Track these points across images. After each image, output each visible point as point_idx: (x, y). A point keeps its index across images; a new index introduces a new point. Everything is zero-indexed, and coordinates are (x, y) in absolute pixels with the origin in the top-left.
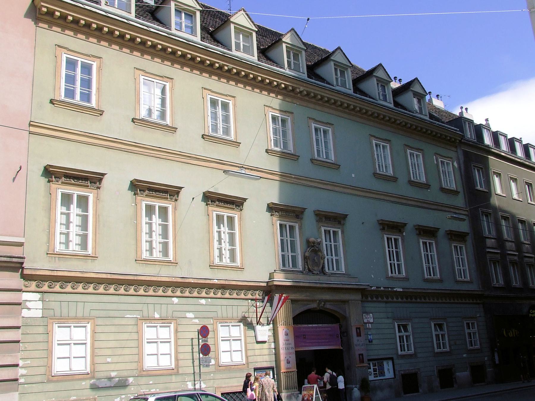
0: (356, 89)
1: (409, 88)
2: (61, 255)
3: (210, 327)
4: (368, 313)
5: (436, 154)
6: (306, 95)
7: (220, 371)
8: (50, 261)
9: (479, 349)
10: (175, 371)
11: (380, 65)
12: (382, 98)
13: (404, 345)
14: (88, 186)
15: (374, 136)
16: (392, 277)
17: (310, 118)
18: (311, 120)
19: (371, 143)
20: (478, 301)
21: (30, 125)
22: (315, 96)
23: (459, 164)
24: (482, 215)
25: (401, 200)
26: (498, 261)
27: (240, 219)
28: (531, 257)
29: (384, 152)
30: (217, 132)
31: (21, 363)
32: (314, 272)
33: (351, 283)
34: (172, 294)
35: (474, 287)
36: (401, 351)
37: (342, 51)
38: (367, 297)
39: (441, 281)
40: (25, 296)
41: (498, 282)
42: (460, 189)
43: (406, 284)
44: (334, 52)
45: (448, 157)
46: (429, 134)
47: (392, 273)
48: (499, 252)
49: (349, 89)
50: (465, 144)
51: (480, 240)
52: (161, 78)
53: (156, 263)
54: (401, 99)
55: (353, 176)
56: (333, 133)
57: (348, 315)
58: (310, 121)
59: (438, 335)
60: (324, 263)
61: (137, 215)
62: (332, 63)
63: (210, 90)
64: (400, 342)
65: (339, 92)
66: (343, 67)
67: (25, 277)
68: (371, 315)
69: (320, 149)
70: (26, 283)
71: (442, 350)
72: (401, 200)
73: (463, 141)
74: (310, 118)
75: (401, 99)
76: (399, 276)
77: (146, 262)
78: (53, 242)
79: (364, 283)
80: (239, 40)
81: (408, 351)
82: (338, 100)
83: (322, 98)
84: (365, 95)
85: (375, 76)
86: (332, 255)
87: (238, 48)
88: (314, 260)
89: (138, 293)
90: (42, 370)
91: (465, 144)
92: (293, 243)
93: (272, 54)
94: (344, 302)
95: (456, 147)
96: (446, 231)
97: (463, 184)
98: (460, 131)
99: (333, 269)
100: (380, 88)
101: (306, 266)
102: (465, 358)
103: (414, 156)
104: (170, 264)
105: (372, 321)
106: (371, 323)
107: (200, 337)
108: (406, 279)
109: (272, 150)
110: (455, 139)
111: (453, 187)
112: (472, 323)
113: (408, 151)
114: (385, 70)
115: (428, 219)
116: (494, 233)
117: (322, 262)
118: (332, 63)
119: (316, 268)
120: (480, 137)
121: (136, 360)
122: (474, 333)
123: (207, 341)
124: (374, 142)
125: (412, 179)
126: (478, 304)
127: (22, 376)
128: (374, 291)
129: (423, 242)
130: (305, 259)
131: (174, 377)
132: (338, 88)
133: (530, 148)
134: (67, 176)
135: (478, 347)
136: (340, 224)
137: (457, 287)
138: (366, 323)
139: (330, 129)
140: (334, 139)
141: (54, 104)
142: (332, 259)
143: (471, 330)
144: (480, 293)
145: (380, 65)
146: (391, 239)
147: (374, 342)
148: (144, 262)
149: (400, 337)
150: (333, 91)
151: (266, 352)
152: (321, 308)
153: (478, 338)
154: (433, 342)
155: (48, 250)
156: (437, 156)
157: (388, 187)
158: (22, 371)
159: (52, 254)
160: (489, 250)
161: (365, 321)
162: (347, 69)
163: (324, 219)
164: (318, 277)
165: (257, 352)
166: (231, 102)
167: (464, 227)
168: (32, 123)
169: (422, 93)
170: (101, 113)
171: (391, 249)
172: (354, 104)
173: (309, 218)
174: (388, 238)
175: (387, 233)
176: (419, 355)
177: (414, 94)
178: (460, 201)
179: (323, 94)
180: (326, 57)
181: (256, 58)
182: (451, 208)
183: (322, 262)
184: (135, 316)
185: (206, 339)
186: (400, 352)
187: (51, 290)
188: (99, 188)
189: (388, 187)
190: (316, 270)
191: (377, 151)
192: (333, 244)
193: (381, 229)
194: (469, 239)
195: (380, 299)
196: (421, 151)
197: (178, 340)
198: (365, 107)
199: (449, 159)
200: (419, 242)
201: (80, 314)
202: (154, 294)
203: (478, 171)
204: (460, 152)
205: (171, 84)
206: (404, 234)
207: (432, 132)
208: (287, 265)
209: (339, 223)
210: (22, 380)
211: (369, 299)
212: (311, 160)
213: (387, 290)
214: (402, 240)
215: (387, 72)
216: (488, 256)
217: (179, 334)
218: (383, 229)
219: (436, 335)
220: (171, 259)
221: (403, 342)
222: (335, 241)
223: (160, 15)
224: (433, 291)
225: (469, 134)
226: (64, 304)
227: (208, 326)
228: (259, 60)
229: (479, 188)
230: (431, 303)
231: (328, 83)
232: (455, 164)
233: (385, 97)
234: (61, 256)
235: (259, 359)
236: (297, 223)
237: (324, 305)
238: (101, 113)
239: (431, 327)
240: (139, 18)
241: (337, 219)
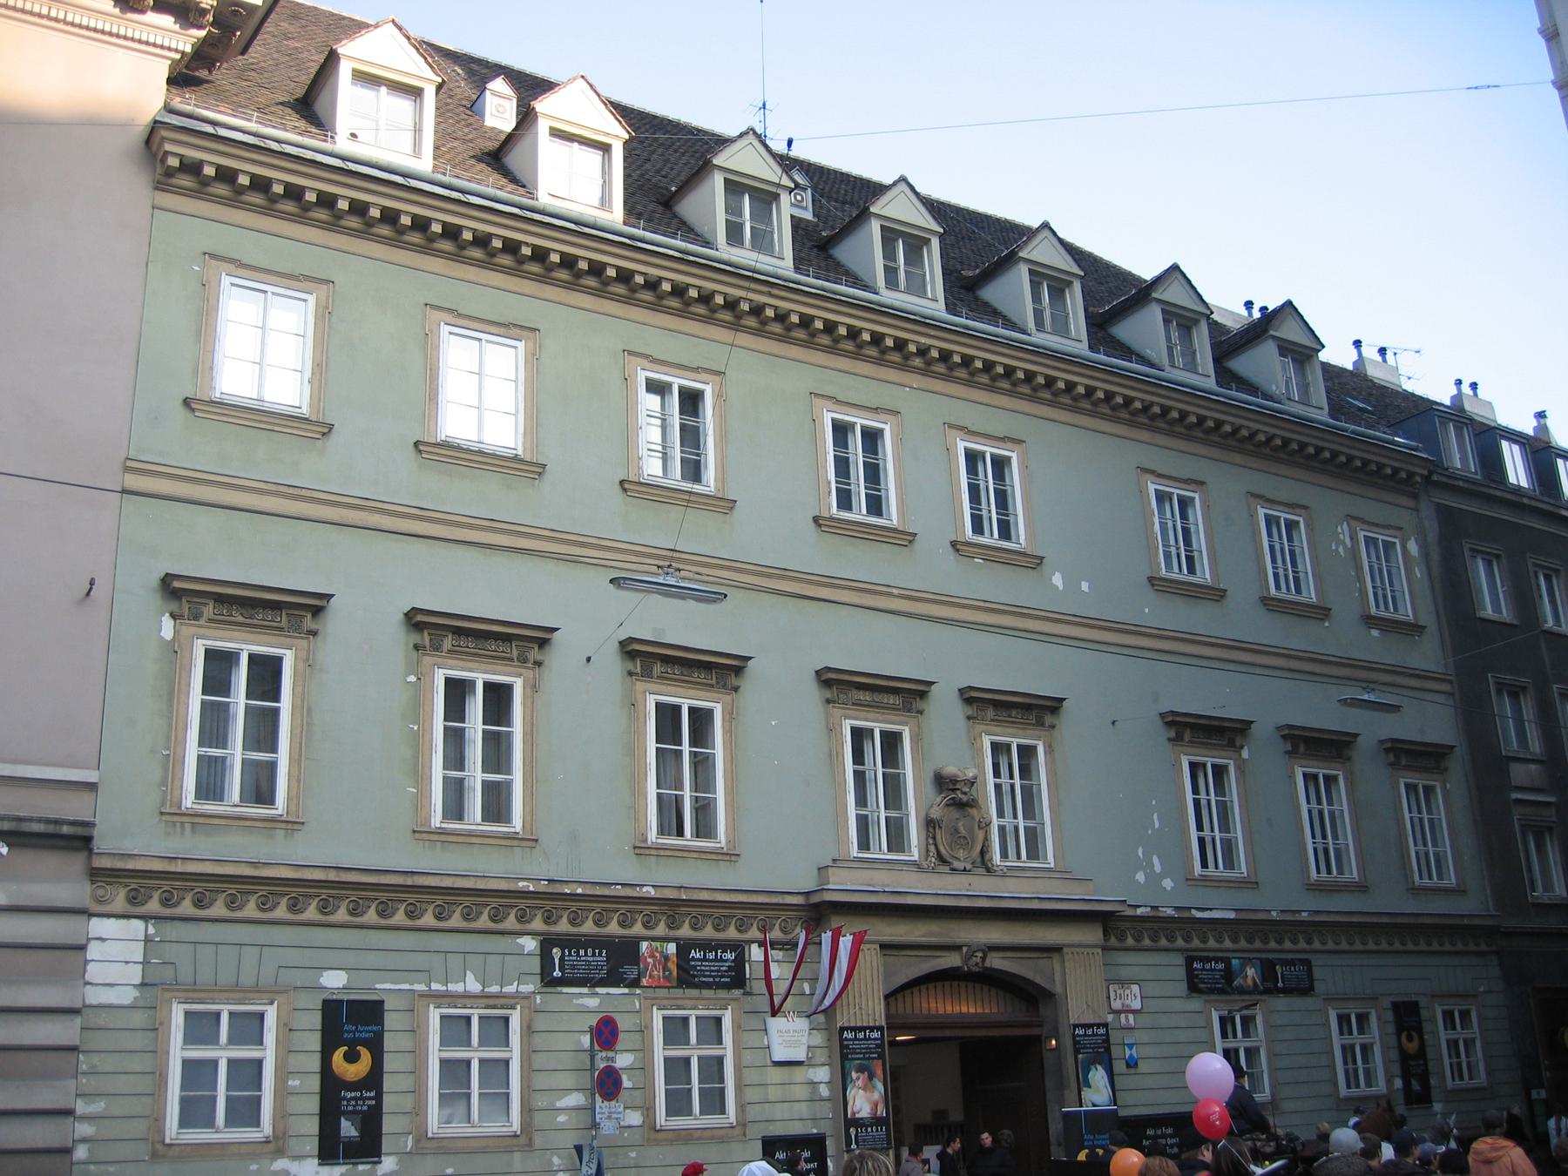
0: (1226, 376)
1: (1266, 331)
2: (197, 821)
3: (623, 1022)
4: (1124, 983)
5: (1350, 518)
6: (1023, 381)
7: (658, 1143)
8: (168, 834)
9: (1484, 1089)
10: (523, 1140)
11: (1175, 268)
12: (1179, 361)
13: (1356, 1071)
14: (281, 629)
15: (1152, 472)
16: (1204, 879)
17: (951, 426)
18: (1148, 476)
19: (1143, 491)
20: (1483, 947)
21: (127, 469)
22: (1146, 408)
23: (1424, 548)
24: (1499, 692)
25: (1236, 654)
26: (1550, 829)
27: (730, 716)
28: (1549, 804)
29: (1290, 539)
30: (849, 508)
31: (81, 1107)
32: (956, 864)
33: (1071, 894)
34: (518, 927)
35: (1474, 905)
36: (1349, 1087)
37: (1054, 233)
38: (1121, 938)
39: (1361, 888)
40: (98, 926)
41: (1548, 886)
42: (1428, 619)
43: (1247, 899)
44: (1158, 281)
45: (1388, 527)
46: (1326, 461)
47: (1204, 865)
48: (1551, 799)
49: (1076, 340)
50: (1438, 484)
51: (1489, 767)
52: (502, 330)
53: (473, 840)
54: (1241, 364)
55: (1085, 586)
56: (1024, 467)
57: (1058, 989)
58: (818, 402)
59: (1456, 1042)
60: (986, 839)
61: (418, 708)
62: (1023, 271)
63: (646, 357)
64: (1345, 1063)
65: (735, 273)
66: (1188, 316)
67: (95, 874)
68: (1135, 988)
69: (984, 513)
70: (100, 892)
71: (1466, 1082)
72: (1236, 654)
73: (1435, 477)
74: (951, 426)
75: (1241, 364)
76: (1229, 874)
77: (443, 838)
78: (177, 783)
79: (1105, 892)
80: (741, 215)
81: (1471, 1078)
82: (660, 279)
83: (989, 366)
84: (1252, 389)
85: (1159, 301)
86: (1015, 817)
87: (892, 283)
88: (957, 831)
89: (331, 919)
90: (139, 1128)
91: (1438, 484)
92: (1224, 810)
93: (845, 252)
94: (1056, 949)
95: (1415, 497)
96: (1382, 742)
97: (1436, 605)
98: (1425, 450)
99: (1019, 857)
100: (1175, 335)
101: (932, 848)
102: (978, 1140)
103: (1376, 547)
104: (515, 843)
105: (1136, 1005)
106: (1134, 1012)
107: (596, 1047)
108: (1250, 884)
109: (832, 519)
110: (1411, 475)
111: (1407, 613)
112: (1461, 1012)
113: (1261, 512)
114: (1189, 281)
115: (1319, 709)
116: (1535, 746)
117: (980, 835)
118: (1023, 271)
119: (961, 854)
120: (1493, 464)
121: (537, 1096)
122: (1469, 1043)
123: (613, 1059)
124: (1152, 488)
125: (1273, 591)
126: (1483, 954)
127: (84, 1140)
128: (1142, 919)
129: (1305, 775)
130: (930, 825)
131: (517, 1156)
132: (1039, 338)
133: (1505, 444)
134: (666, 660)
135: (1481, 1079)
136: (1042, 725)
137: (1411, 906)
138: (1118, 1012)
139: (1196, 496)
140: (1234, 527)
141: (193, 410)
142: (1016, 828)
143: (1460, 1034)
144: (1489, 922)
145: (1175, 268)
146: (1204, 765)
147: (1143, 1067)
148: (436, 837)
149: (1344, 1048)
150: (1158, 385)
151: (801, 1092)
152: (976, 969)
153: (1480, 1054)
154: (1332, 1067)
155: (163, 804)
156: (1354, 523)
157: (1299, 636)
158: (84, 1129)
159: (173, 816)
160: (1519, 796)
161: (1117, 1005)
162: (1196, 322)
163: (1302, 748)
164: (970, 879)
165: (773, 1093)
166: (1014, 456)
167: (1431, 721)
168: (129, 464)
169: (1308, 343)
170: (328, 430)
171: (1415, 815)
172: (1163, 401)
173: (944, 709)
174: (1192, 765)
175: (1189, 750)
176: (1287, 1106)
177: (1280, 348)
178: (1427, 654)
179: (1366, 456)
180: (1138, 293)
181: (942, 304)
182: (1330, 663)
183: (980, 835)
184: (406, 986)
185: (610, 1054)
186: (1343, 1091)
187: (441, 924)
188: (736, 689)
189: (1299, 636)
190: (962, 858)
191: (1270, 535)
192: (1426, 816)
193: (1170, 740)
194: (1457, 767)
195: (1163, 942)
196: (1303, 512)
197: (534, 1056)
198: (751, 296)
199: (1391, 532)
200: (1292, 777)
201: (248, 979)
202: (464, 925)
203: (1489, 564)
204: (1427, 511)
205: (531, 344)
206: (1245, 754)
207: (1319, 450)
208: (1346, 870)
209: (1040, 723)
210: (81, 1153)
211: (1130, 941)
212: (622, 482)
213: (1185, 914)
214: (1238, 768)
215: (1194, 288)
216: (1517, 814)
217: (537, 1039)
218: (1177, 740)
219: (1448, 1041)
220: (519, 828)
221: (1355, 1062)
222: (1429, 811)
223: (513, 160)
224: (1393, 920)
225: (1459, 456)
226: (206, 952)
227: (616, 1017)
228: (797, 269)
229: (1488, 612)
230: (1457, 953)
231: (1152, 365)
232: (1413, 547)
233: (1304, 388)
234: (201, 820)
235: (780, 1111)
236: (905, 724)
237: (984, 959)
238: (328, 430)
239: (1327, 1024)
240: (1098, 352)
241: (1038, 710)
